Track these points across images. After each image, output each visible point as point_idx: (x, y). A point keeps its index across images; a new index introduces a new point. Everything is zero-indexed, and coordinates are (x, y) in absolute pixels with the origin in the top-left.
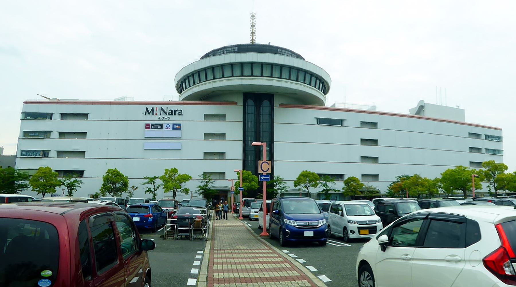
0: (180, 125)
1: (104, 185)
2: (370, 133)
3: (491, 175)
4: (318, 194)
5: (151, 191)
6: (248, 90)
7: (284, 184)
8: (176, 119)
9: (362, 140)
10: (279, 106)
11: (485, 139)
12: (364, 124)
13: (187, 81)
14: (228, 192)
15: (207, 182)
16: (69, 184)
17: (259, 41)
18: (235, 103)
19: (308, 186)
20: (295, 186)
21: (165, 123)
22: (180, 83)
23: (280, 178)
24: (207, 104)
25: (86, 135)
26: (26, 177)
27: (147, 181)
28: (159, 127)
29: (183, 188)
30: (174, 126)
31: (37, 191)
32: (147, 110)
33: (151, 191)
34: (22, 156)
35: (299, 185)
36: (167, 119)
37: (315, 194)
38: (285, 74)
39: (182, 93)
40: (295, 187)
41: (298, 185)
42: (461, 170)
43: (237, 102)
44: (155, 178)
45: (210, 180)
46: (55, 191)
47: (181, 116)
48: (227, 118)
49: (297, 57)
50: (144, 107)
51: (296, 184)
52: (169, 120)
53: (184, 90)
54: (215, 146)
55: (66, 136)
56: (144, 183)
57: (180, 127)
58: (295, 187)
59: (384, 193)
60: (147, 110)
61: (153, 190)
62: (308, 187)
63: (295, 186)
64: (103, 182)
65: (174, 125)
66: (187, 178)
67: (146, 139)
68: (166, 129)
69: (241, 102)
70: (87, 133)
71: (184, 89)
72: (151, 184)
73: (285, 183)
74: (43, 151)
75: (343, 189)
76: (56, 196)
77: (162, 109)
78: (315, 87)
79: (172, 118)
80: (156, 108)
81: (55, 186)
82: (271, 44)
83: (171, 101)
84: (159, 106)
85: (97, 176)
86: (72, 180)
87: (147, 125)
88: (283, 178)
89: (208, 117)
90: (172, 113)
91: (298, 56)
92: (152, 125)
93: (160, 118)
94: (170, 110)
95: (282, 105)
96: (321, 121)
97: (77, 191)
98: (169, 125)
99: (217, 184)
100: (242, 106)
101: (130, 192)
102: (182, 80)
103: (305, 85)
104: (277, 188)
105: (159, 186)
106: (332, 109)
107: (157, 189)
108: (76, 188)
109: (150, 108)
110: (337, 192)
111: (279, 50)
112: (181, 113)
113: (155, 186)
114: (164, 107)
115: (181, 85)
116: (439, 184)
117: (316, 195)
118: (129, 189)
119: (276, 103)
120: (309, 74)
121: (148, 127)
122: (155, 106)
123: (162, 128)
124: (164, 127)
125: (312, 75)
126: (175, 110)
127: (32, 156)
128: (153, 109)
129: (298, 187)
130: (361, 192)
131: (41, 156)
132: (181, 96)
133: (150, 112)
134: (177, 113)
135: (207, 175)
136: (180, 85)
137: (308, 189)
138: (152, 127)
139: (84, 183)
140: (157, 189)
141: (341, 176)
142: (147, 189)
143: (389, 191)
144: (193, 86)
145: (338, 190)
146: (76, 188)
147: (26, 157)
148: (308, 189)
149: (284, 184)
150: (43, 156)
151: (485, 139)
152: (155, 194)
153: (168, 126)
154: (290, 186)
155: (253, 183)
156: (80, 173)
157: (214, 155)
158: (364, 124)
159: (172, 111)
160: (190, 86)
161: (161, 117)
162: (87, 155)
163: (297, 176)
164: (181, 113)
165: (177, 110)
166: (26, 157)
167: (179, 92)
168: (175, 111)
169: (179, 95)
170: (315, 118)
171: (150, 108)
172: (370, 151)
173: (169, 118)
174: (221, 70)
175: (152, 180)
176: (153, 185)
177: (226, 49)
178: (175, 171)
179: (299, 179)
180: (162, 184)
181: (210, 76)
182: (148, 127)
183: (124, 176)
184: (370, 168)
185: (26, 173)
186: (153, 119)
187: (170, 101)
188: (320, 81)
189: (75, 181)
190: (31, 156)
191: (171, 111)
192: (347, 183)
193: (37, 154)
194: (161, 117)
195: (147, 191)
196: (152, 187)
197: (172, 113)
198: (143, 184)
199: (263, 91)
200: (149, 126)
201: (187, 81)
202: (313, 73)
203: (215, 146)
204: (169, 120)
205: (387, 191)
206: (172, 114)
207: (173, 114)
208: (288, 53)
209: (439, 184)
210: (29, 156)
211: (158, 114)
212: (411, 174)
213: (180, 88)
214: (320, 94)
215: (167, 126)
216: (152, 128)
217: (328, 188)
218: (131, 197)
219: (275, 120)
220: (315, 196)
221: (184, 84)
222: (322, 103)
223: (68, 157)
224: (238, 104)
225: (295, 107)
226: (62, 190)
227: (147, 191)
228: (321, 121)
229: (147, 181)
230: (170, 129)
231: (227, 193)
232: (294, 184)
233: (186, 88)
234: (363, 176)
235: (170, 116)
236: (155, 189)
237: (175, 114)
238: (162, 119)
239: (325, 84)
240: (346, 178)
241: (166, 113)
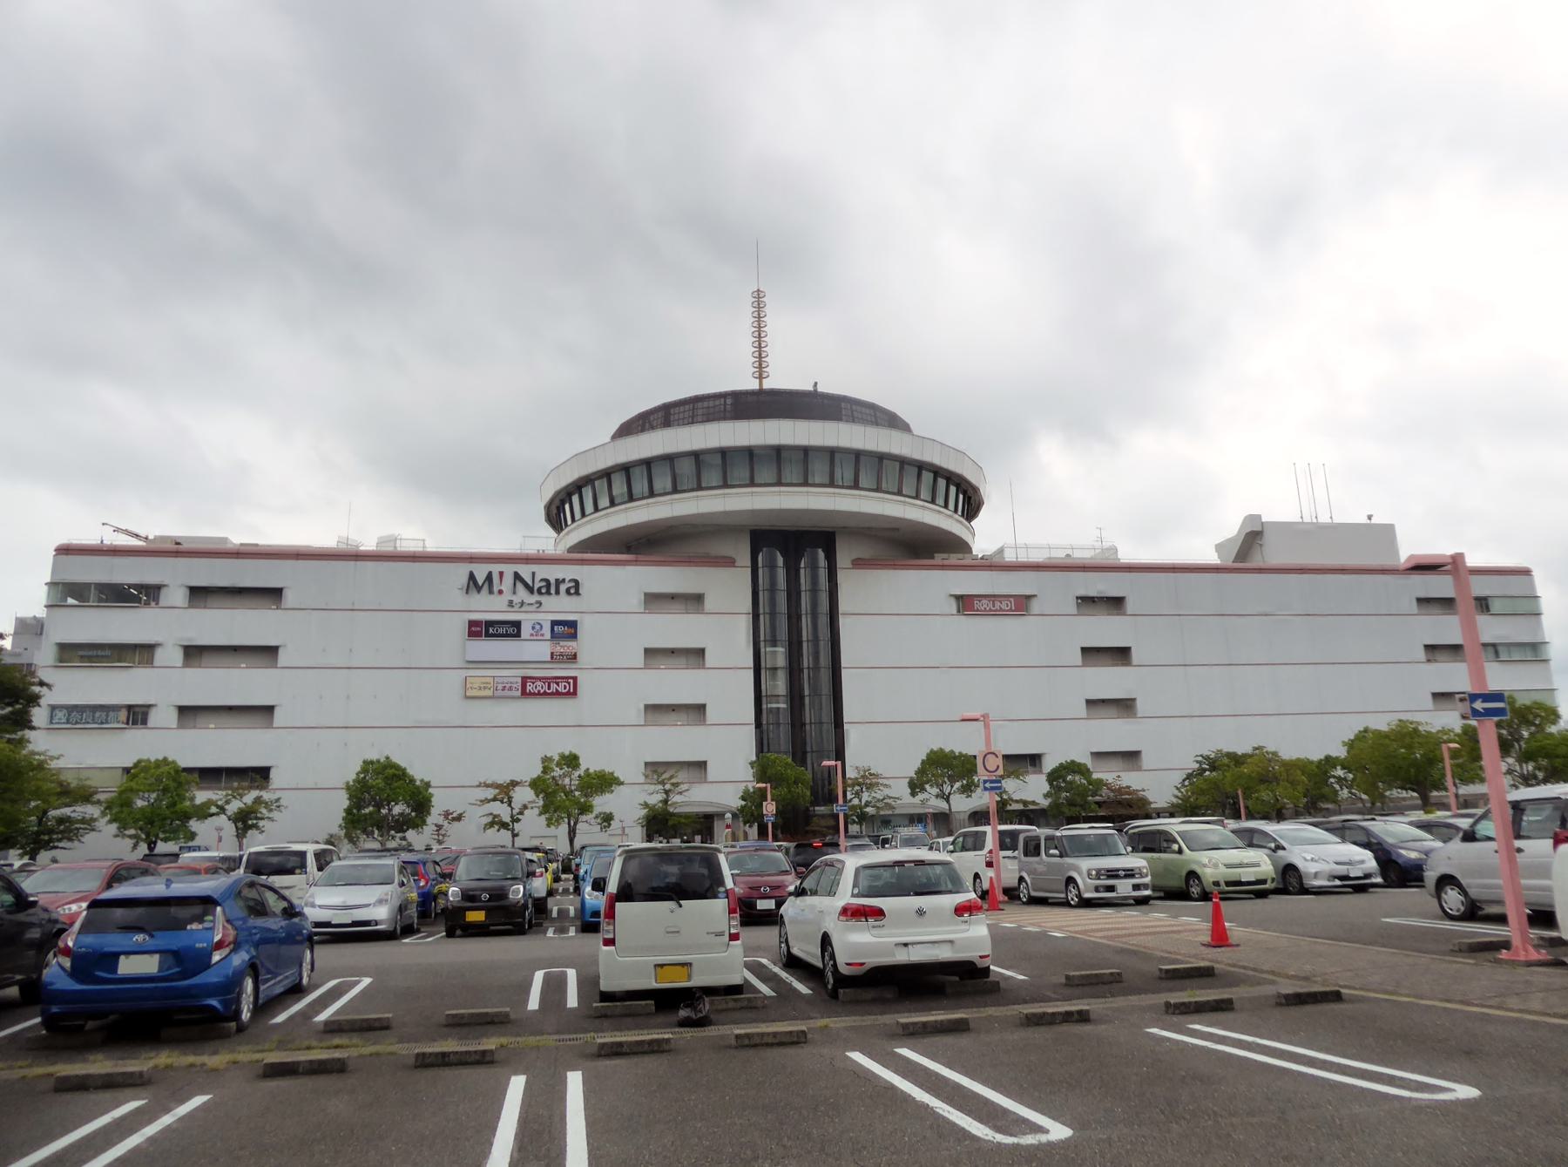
0: (573, 625)
1: (348, 811)
2: (1106, 630)
3: (1505, 747)
4: (971, 814)
5: (504, 825)
6: (764, 524)
7: (882, 791)
8: (559, 607)
9: (1085, 650)
10: (851, 566)
11: (955, 612)
12: (1088, 602)
13: (575, 499)
14: (715, 818)
15: (667, 792)
16: (241, 811)
17: (778, 380)
18: (729, 562)
19: (950, 794)
20: (913, 794)
21: (527, 619)
22: (557, 502)
23: (872, 772)
24: (636, 562)
25: (277, 659)
26: (86, 796)
27: (490, 793)
28: (510, 630)
29: (597, 810)
30: (556, 628)
31: (130, 837)
32: (472, 577)
33: (504, 825)
34: (51, 723)
35: (923, 790)
36: (533, 608)
37: (962, 815)
38: (819, 470)
39: (564, 532)
40: (914, 797)
41: (131, 768)
42: (1407, 735)
43: (734, 556)
44: (514, 784)
45: (676, 785)
46: (193, 836)
47: (574, 598)
48: (709, 604)
49: (889, 426)
50: (462, 571)
51: (915, 786)
52: (542, 609)
53: (576, 519)
54: (677, 685)
55: (206, 659)
56: (481, 801)
57: (573, 631)
58: (914, 797)
59: (1166, 805)
60: (472, 577)
61: (507, 819)
62: (948, 797)
63: (913, 794)
64: (346, 804)
65: (554, 623)
66: (604, 782)
67: (471, 666)
68: (532, 635)
69: (744, 558)
70: (281, 651)
71: (569, 522)
72: (502, 802)
73: (886, 786)
74: (130, 708)
75: (1046, 796)
76: (198, 849)
77: (517, 576)
78: (946, 506)
79: (550, 602)
80: (501, 574)
81: (186, 817)
82: (820, 389)
83: (543, 551)
84: (509, 570)
85: (316, 784)
86: (250, 797)
87: (472, 624)
88: (879, 772)
89: (654, 600)
90: (548, 588)
91: (892, 421)
92: (490, 624)
93: (511, 603)
94: (542, 580)
95: (858, 563)
96: (965, 603)
97: (263, 832)
98: (539, 624)
99: (694, 798)
100: (750, 569)
101: (439, 827)
102: (563, 495)
103: (862, 493)
104: (863, 804)
105: (525, 807)
106: (992, 565)
107: (520, 817)
108: (261, 823)
109: (481, 573)
110: (1031, 807)
111: (843, 405)
112: (575, 589)
113: (512, 809)
114: (525, 571)
115: (561, 509)
116: (1339, 772)
117: (967, 817)
118: (434, 818)
119: (843, 558)
120: (930, 471)
121: (480, 630)
122: (495, 568)
123: (518, 635)
124: (526, 631)
125: (937, 472)
126: (557, 580)
127: (88, 723)
128: (489, 578)
129: (921, 797)
130: (1099, 804)
131: (123, 723)
132: (561, 540)
133: (483, 585)
134: (563, 588)
135: (655, 769)
136: (558, 508)
137: (948, 800)
138: (487, 631)
139: (286, 807)
140: (520, 817)
141: (1034, 760)
142: (490, 819)
143: (1180, 802)
144: (592, 513)
145: (1033, 803)
146: (261, 823)
147: (96, 726)
148: (948, 800)
149: (882, 791)
150: (128, 723)
151: (959, 611)
152: (516, 832)
153: (538, 627)
154: (899, 793)
155: (800, 789)
156: (261, 775)
157: (673, 710)
158: (1088, 602)
159: (547, 581)
160: (596, 509)
161: (517, 600)
162: (279, 717)
163: (918, 764)
164: (575, 589)
165: (564, 580)
166: (96, 726)
167: (554, 527)
168: (558, 582)
169: (556, 535)
170: (951, 595)
171: (481, 573)
172: (1109, 681)
173: (541, 604)
174: (775, 471)
175: (505, 791)
176: (506, 805)
177: (700, 404)
178: (571, 761)
179: (921, 772)
180: (533, 802)
181: (640, 486)
182: (480, 630)
183: (418, 783)
184: (1114, 733)
185: (86, 780)
186: (491, 607)
187: (541, 552)
188: (958, 486)
189: (258, 800)
190: (84, 723)
191: (573, 584)
192: (1054, 777)
193: (107, 716)
194: (517, 600)
195: (491, 825)
196: (503, 812)
197: (548, 588)
198: (479, 803)
199: (805, 524)
200: (479, 629)
201: (575, 499)
202: (941, 468)
203: (677, 685)
204: (539, 610)
205: (1175, 800)
206: (548, 593)
207: (553, 591)
208: (868, 411)
209: (1339, 772)
210: (77, 723)
211: (503, 595)
212: (1242, 748)
213: (556, 516)
214: (959, 525)
215: (533, 628)
216: (488, 635)
217: (1005, 797)
218: (440, 842)
219: (844, 605)
220: (964, 820)
221: (567, 507)
222: (961, 546)
223: (215, 724)
224: (736, 564)
225: (895, 567)
226: (217, 829)
227: (491, 825)
228: (965, 603)
229: (490, 793)
230: (542, 635)
231: (713, 822)
232: (909, 791)
233: (573, 520)
234: (1098, 755)
235: (543, 599)
236: (512, 816)
237: (557, 592)
238: (519, 605)
239: (970, 492)
240: (1049, 764)
241: (530, 589)
